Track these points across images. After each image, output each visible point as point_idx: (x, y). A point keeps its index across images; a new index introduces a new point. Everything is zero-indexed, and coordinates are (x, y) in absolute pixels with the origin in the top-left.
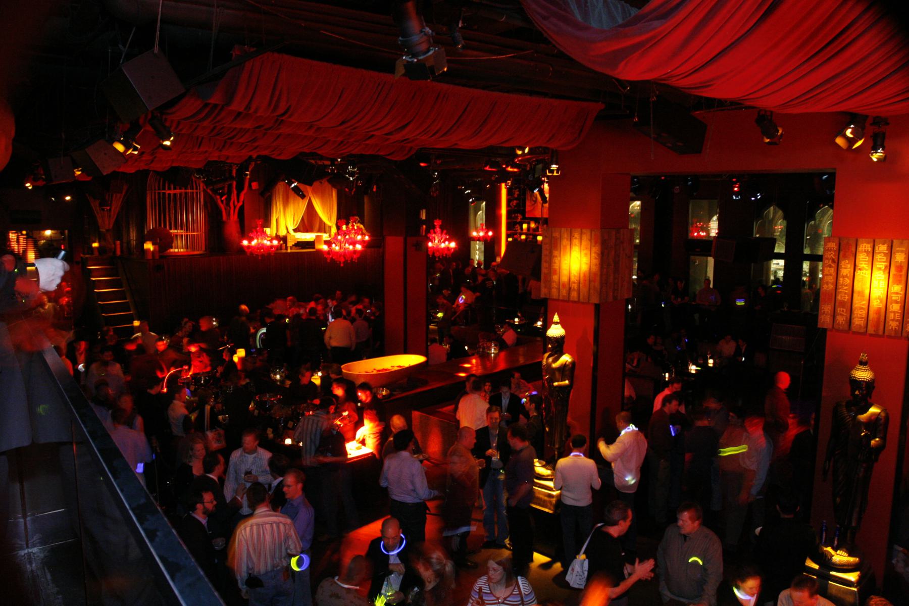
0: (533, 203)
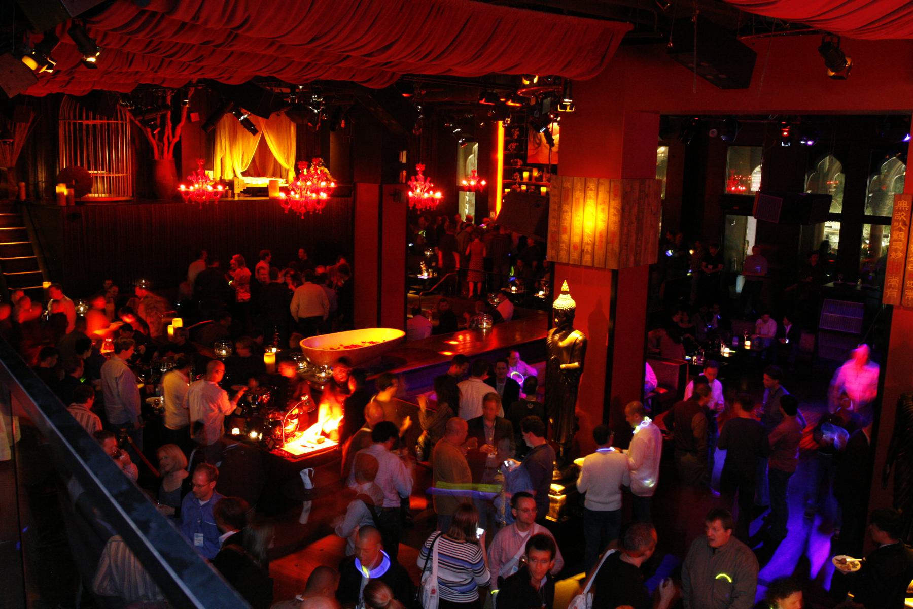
0: (537, 146)
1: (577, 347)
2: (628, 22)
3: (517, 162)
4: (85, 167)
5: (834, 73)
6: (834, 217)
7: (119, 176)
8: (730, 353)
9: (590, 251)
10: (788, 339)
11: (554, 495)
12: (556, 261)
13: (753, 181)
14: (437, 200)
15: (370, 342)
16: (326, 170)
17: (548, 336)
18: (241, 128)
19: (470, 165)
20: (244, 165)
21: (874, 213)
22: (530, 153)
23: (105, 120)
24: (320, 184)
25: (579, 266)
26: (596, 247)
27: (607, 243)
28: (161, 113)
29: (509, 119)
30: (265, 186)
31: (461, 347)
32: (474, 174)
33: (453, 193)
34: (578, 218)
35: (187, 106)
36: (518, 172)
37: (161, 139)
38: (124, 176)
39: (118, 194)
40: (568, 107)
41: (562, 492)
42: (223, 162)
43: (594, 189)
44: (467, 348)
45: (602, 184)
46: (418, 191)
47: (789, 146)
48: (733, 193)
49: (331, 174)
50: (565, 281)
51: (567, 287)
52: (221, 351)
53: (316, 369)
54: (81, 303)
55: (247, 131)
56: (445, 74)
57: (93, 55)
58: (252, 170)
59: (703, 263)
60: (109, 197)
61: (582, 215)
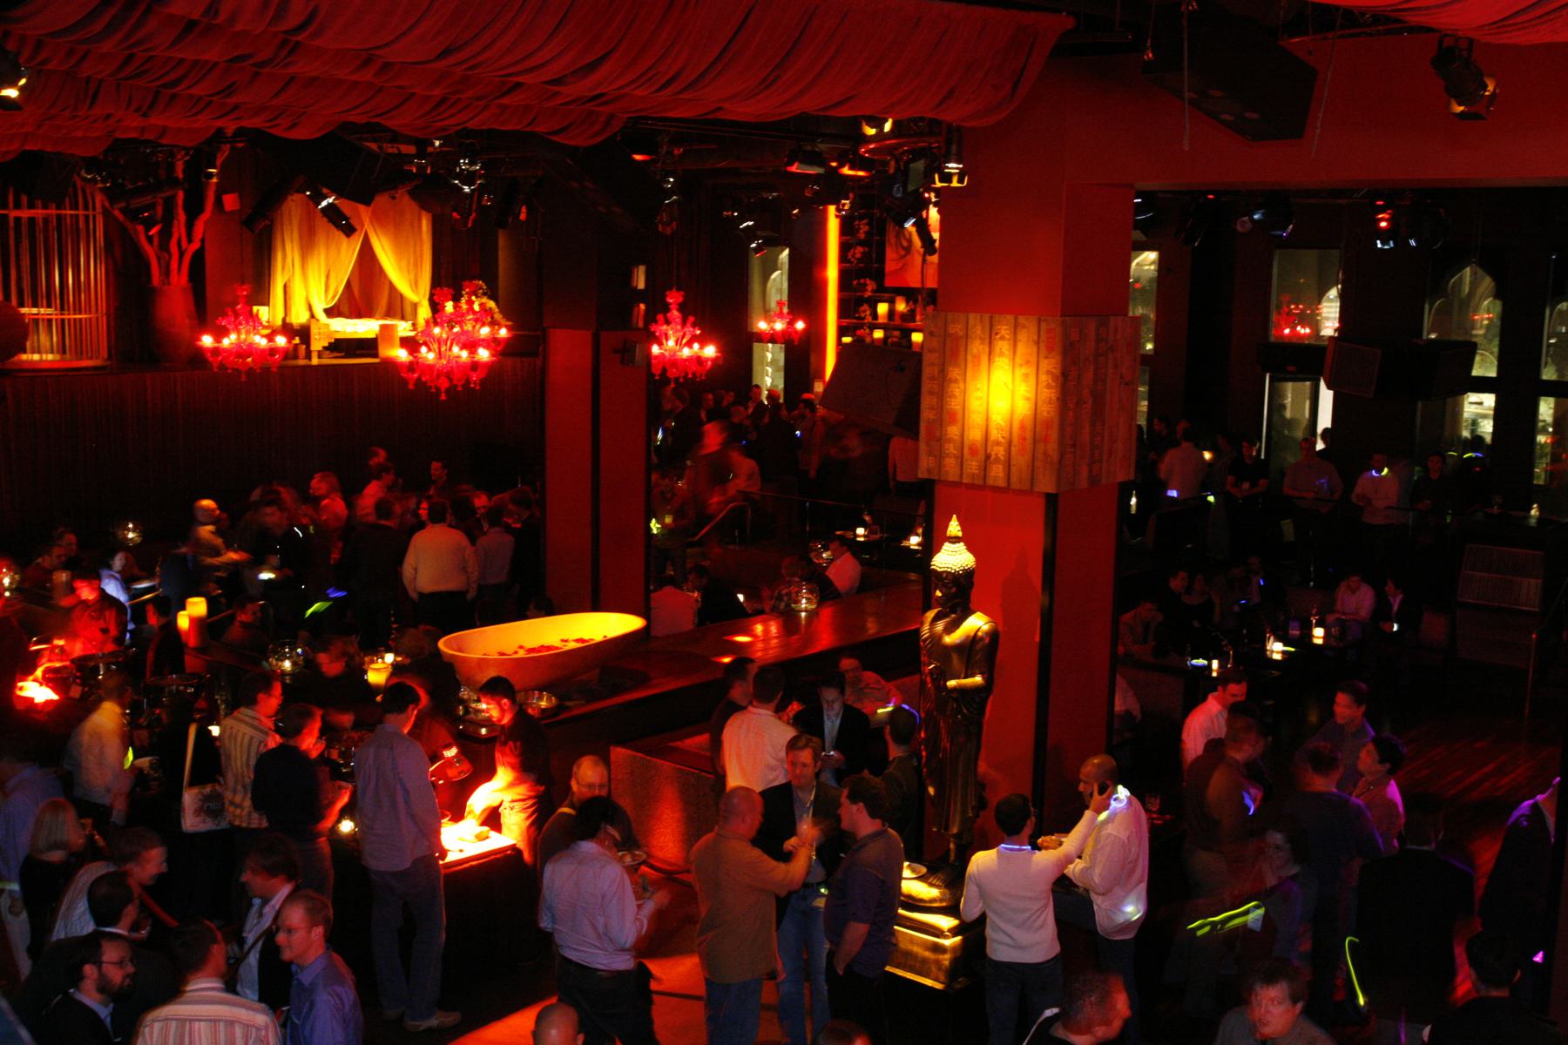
0: (903, 253)
1: (979, 647)
2: (1064, 14)
3: (866, 285)
4: (14, 302)
5: (1462, 108)
6: (1482, 385)
7: (81, 319)
8: (1284, 653)
9: (1002, 458)
10: (1397, 623)
11: (938, 937)
12: (936, 478)
13: (1324, 315)
14: (707, 360)
15: (578, 641)
16: (491, 304)
17: (922, 623)
18: (322, 224)
19: (773, 291)
20: (330, 296)
21: (1559, 376)
22: (890, 265)
23: (52, 209)
24: (479, 331)
25: (981, 487)
26: (1013, 449)
27: (1035, 441)
28: (163, 195)
29: (848, 202)
30: (372, 335)
31: (760, 645)
32: (781, 309)
33: (740, 346)
34: (979, 394)
35: (215, 180)
36: (867, 303)
37: (164, 246)
38: (90, 319)
39: (79, 354)
40: (955, 179)
41: (955, 932)
42: (288, 289)
43: (1007, 337)
44: (773, 648)
45: (1024, 327)
46: (671, 343)
47: (1392, 248)
48: (1286, 341)
49: (501, 312)
50: (955, 516)
51: (959, 528)
52: (282, 660)
54: (4, 570)
55: (335, 229)
56: (711, 116)
57: (13, 84)
58: (346, 306)
59: (1230, 477)
60: (62, 361)
61: (985, 388)
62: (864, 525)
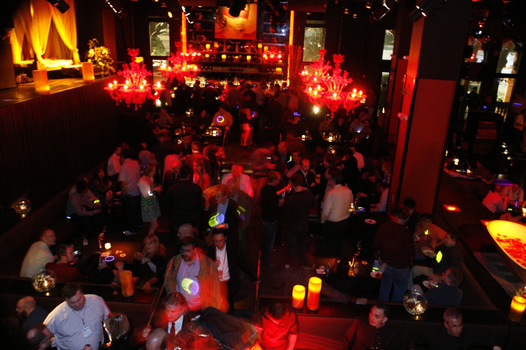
0: (223, 26)
53: (356, 198)
62: (305, 134)
